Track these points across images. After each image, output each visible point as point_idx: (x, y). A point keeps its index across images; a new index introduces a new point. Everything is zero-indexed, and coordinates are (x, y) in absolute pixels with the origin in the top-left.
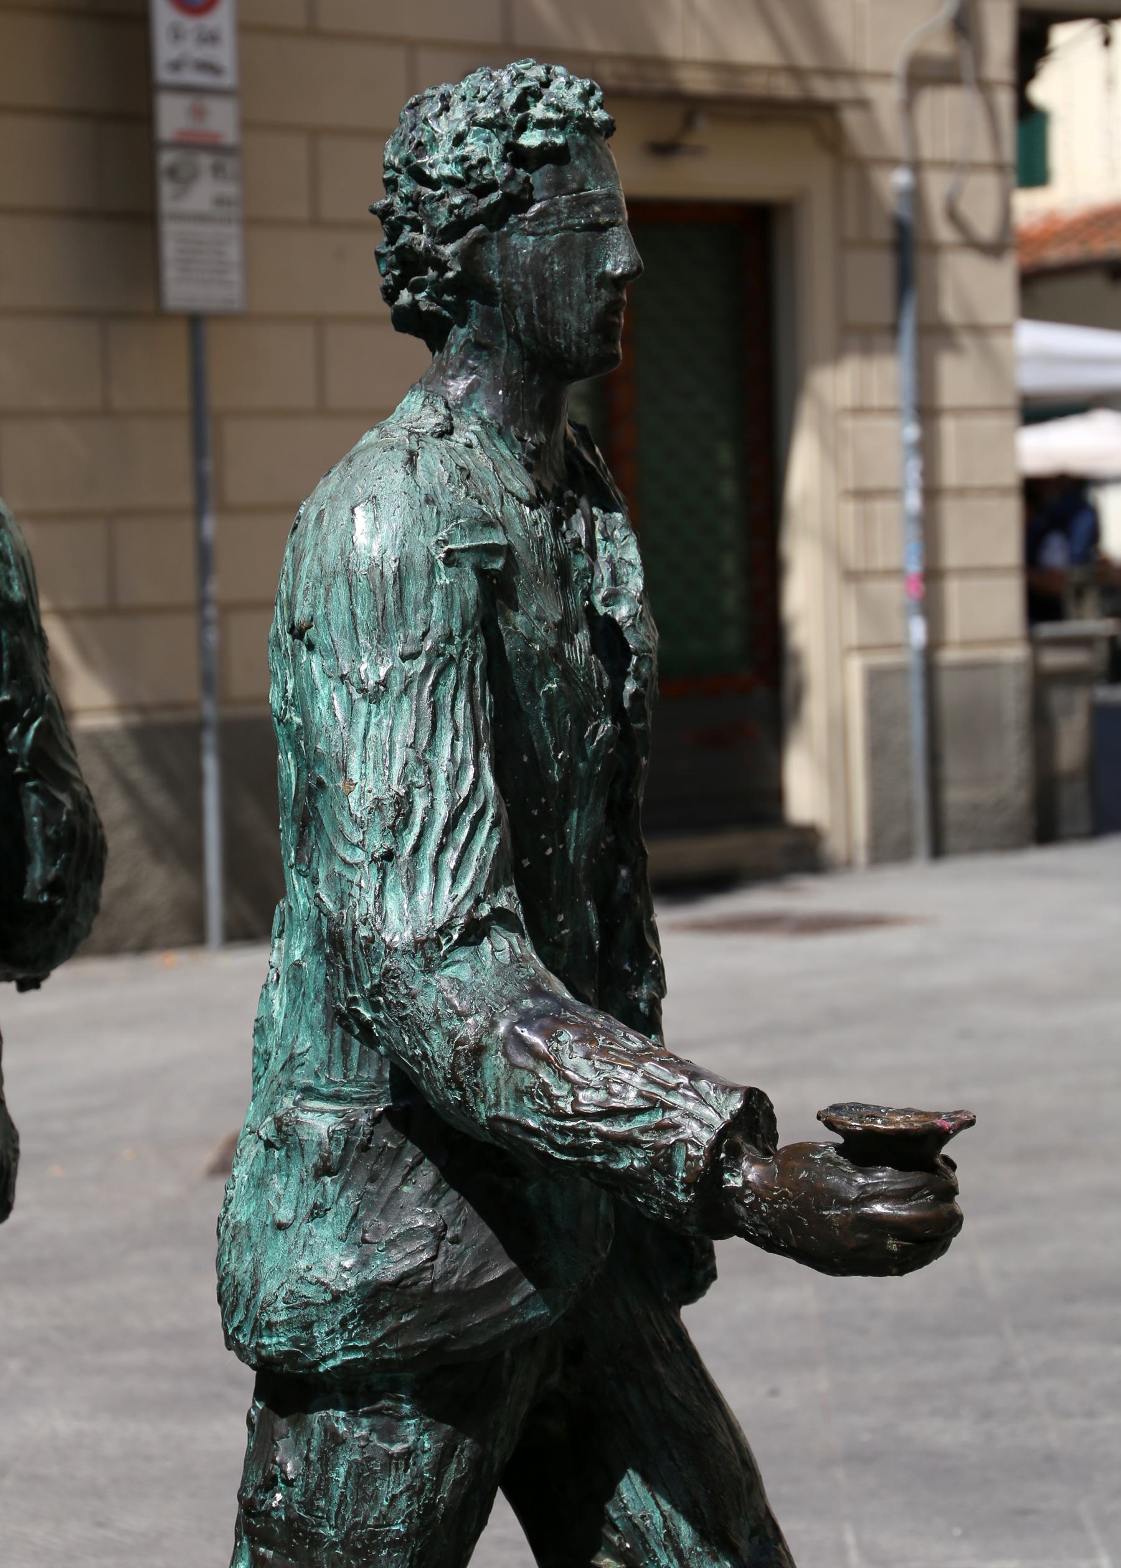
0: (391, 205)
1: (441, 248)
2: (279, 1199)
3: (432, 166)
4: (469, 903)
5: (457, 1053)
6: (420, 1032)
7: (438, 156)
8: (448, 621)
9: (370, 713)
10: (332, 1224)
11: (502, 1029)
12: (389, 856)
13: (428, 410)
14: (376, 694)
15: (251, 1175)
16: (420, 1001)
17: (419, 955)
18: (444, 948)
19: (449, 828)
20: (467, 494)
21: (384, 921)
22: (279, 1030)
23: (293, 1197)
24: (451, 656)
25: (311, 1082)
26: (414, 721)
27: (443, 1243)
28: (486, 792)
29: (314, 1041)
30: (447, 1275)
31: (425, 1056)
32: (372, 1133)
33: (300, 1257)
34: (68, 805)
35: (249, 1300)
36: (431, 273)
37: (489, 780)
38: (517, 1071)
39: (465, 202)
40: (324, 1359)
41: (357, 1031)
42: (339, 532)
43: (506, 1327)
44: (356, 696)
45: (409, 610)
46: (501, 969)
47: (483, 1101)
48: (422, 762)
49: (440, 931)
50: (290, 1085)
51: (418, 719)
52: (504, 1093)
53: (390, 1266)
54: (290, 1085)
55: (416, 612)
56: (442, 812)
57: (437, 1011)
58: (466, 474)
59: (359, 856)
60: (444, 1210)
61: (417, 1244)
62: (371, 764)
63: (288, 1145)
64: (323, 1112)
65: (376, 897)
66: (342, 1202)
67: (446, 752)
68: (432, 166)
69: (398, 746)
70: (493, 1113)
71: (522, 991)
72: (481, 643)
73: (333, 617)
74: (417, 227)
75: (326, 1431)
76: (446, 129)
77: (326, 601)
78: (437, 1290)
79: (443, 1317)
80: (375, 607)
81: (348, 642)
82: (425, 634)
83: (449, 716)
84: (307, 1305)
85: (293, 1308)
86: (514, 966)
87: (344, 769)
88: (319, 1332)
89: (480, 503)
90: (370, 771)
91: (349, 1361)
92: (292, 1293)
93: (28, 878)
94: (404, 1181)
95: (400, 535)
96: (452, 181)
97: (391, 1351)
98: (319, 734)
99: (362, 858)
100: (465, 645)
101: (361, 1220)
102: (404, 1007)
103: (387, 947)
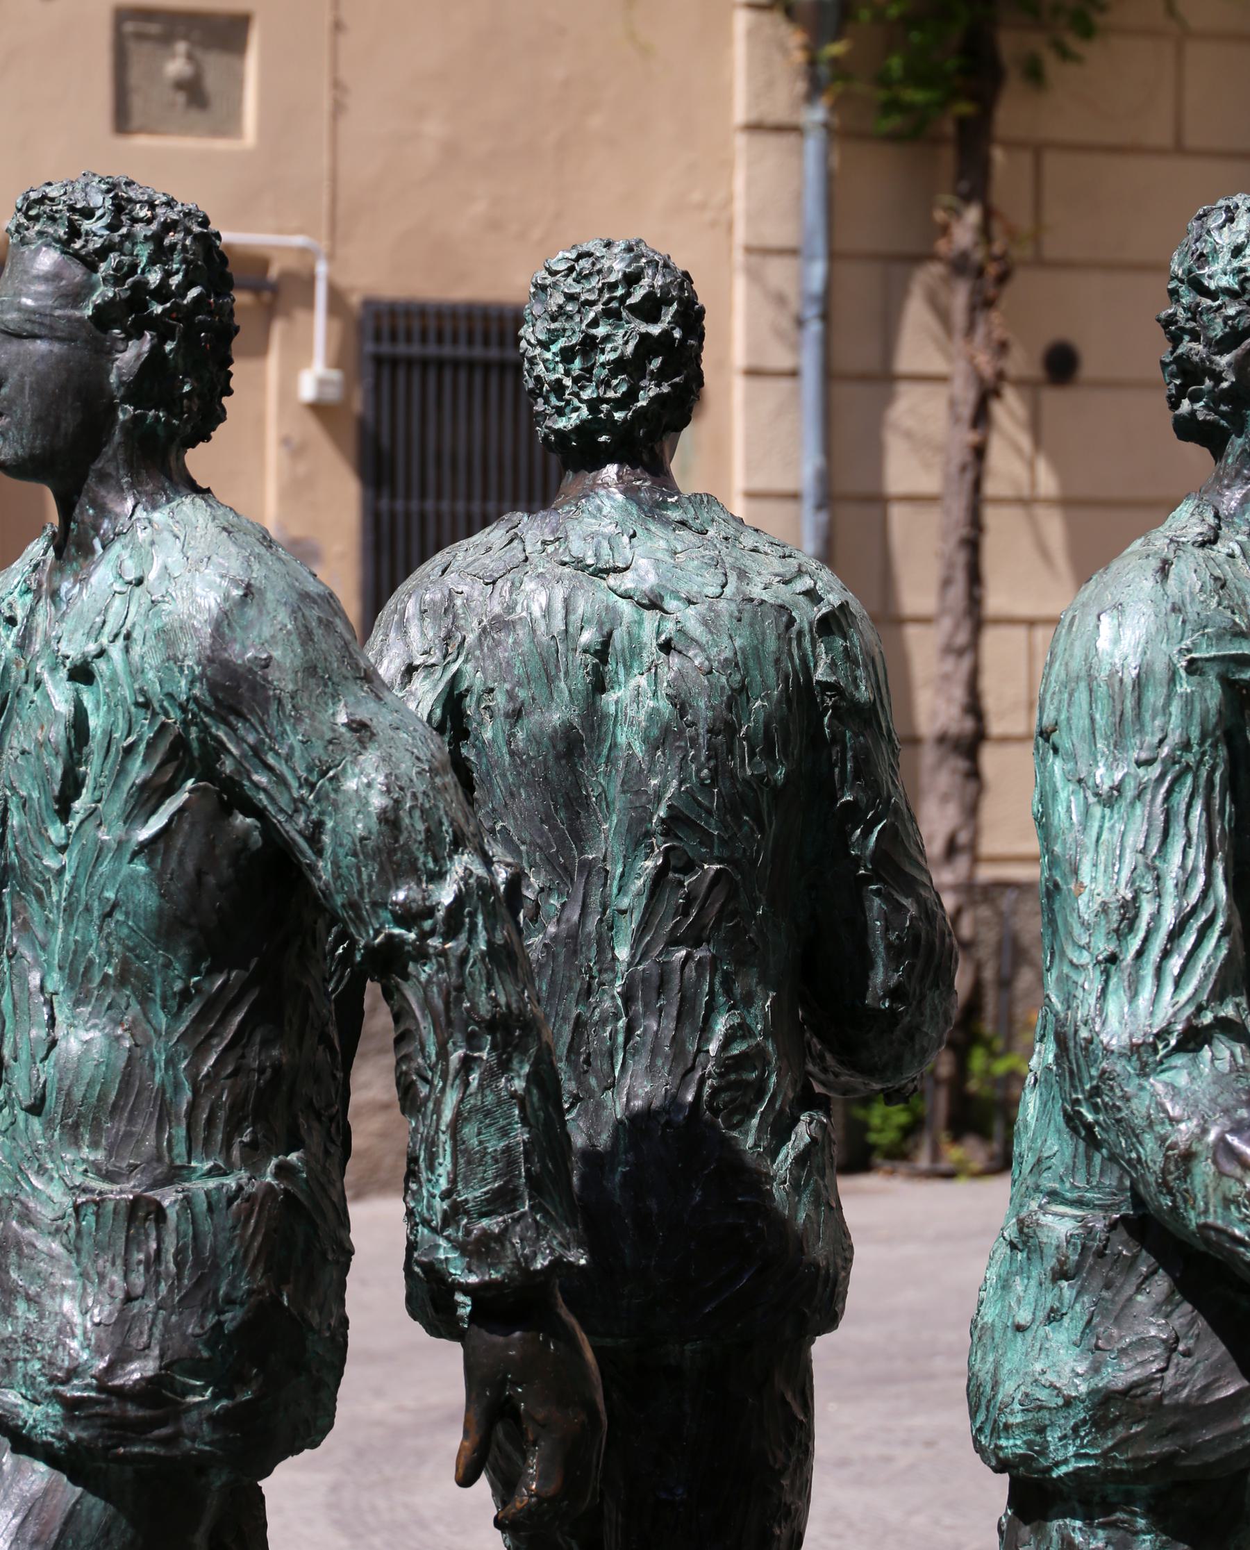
0: (1175, 314)
1: (1217, 358)
2: (1019, 1301)
3: (1210, 277)
4: (1190, 1010)
5: (1167, 1158)
6: (1134, 1135)
7: (1216, 267)
8: (1186, 729)
9: (1103, 817)
10: (1067, 1329)
11: (1212, 1137)
12: (1113, 959)
13: (1195, 520)
14: (1109, 800)
15: (999, 1276)
16: (1134, 1104)
17: (1135, 1058)
18: (1162, 1053)
19: (1176, 934)
20: (1219, 604)
21: (1104, 1023)
22: (1030, 1134)
23: (1032, 1300)
24: (1188, 764)
25: (1057, 1186)
26: (1145, 827)
27: (1174, 1355)
28: (1216, 901)
29: (1061, 1145)
30: (1177, 1388)
31: (1139, 1158)
32: (1108, 1239)
33: (1037, 1359)
34: (913, 911)
35: (989, 1401)
36: (1208, 383)
37: (1221, 889)
38: (1225, 1179)
39: (1239, 313)
40: (1057, 1464)
41: (1083, 1133)
42: (1085, 638)
43: (1237, 1446)
44: (1092, 799)
45: (1147, 716)
46: (1219, 1078)
47: (1193, 1208)
48: (1151, 868)
49: (1158, 1036)
50: (1037, 1189)
51: (1150, 825)
52: (1212, 1201)
53: (1118, 1375)
54: (1037, 1189)
55: (1153, 719)
56: (1169, 920)
57: (1149, 1116)
58: (1222, 583)
59: (1085, 958)
60: (1177, 1321)
61: (1147, 1355)
62: (1101, 867)
63: (1029, 1248)
64: (1063, 1216)
65: (1098, 998)
66: (1078, 1307)
67: (1176, 859)
68: (1210, 277)
69: (1128, 851)
70: (1202, 1220)
71: (1237, 1100)
72: (1223, 752)
73: (1074, 721)
74: (1195, 337)
75: (1063, 1540)
76: (1227, 241)
77: (1069, 705)
78: (1166, 1402)
79: (1173, 1430)
80: (1113, 712)
81: (1086, 746)
82: (1161, 741)
83: (1182, 823)
84: (1040, 1408)
85: (1027, 1410)
86: (1233, 1076)
87: (1075, 871)
88: (1053, 1436)
89: (1233, 613)
90: (1100, 875)
91: (1080, 1469)
92: (1027, 1395)
93: (870, 984)
94: (1139, 1290)
95: (1142, 641)
96: (1228, 292)
97: (1121, 1461)
98: (1057, 837)
99: (1088, 960)
100: (1204, 754)
101: (1095, 1327)
102: (1119, 1109)
103: (1105, 1049)
